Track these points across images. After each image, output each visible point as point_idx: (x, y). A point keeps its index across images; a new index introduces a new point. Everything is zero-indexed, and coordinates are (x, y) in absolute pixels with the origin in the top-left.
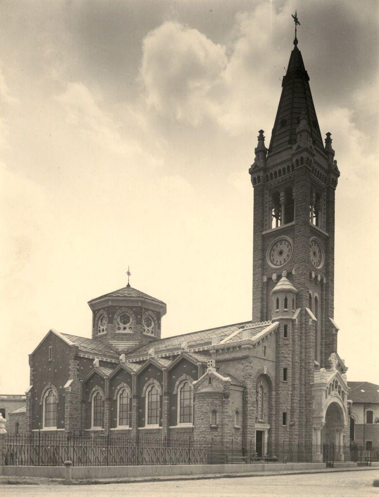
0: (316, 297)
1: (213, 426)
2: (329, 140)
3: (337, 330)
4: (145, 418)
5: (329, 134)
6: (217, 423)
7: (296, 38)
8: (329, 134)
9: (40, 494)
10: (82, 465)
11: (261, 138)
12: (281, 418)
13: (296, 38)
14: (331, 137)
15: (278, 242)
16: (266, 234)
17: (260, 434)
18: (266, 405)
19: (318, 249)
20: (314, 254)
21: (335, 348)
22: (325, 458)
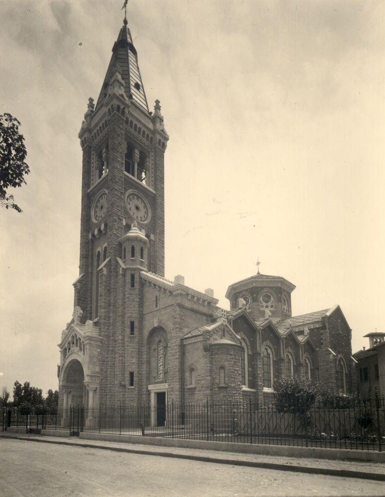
0: (99, 252)
1: (221, 385)
2: (158, 107)
3: (75, 285)
4: (249, 380)
5: (157, 102)
6: (226, 382)
7: (125, 18)
8: (157, 102)
9: (128, 495)
10: (236, 441)
11: (91, 100)
12: (135, 379)
13: (125, 18)
14: (160, 104)
15: (99, 198)
16: (95, 187)
17: (161, 396)
18: (153, 364)
19: (143, 205)
20: (137, 208)
21: (76, 300)
22: (70, 425)
